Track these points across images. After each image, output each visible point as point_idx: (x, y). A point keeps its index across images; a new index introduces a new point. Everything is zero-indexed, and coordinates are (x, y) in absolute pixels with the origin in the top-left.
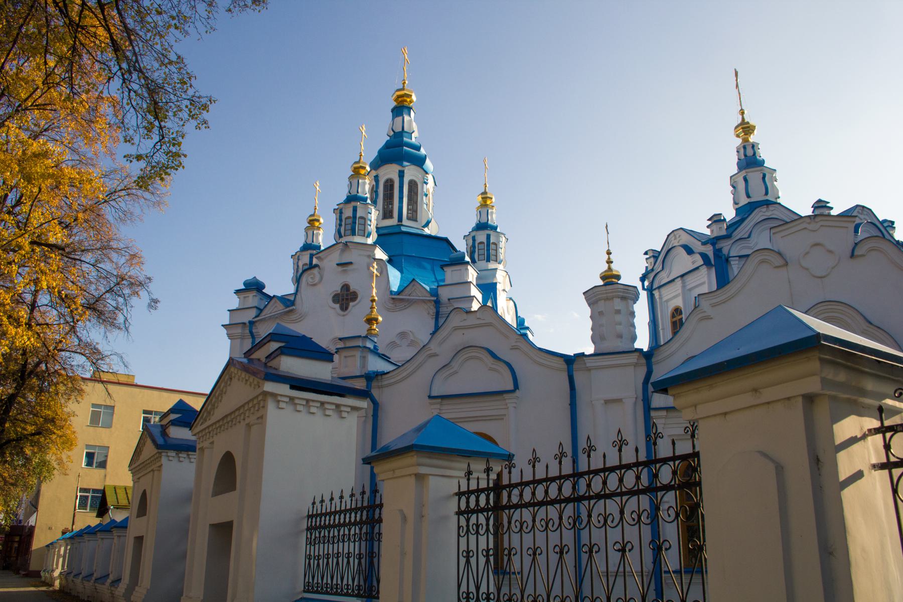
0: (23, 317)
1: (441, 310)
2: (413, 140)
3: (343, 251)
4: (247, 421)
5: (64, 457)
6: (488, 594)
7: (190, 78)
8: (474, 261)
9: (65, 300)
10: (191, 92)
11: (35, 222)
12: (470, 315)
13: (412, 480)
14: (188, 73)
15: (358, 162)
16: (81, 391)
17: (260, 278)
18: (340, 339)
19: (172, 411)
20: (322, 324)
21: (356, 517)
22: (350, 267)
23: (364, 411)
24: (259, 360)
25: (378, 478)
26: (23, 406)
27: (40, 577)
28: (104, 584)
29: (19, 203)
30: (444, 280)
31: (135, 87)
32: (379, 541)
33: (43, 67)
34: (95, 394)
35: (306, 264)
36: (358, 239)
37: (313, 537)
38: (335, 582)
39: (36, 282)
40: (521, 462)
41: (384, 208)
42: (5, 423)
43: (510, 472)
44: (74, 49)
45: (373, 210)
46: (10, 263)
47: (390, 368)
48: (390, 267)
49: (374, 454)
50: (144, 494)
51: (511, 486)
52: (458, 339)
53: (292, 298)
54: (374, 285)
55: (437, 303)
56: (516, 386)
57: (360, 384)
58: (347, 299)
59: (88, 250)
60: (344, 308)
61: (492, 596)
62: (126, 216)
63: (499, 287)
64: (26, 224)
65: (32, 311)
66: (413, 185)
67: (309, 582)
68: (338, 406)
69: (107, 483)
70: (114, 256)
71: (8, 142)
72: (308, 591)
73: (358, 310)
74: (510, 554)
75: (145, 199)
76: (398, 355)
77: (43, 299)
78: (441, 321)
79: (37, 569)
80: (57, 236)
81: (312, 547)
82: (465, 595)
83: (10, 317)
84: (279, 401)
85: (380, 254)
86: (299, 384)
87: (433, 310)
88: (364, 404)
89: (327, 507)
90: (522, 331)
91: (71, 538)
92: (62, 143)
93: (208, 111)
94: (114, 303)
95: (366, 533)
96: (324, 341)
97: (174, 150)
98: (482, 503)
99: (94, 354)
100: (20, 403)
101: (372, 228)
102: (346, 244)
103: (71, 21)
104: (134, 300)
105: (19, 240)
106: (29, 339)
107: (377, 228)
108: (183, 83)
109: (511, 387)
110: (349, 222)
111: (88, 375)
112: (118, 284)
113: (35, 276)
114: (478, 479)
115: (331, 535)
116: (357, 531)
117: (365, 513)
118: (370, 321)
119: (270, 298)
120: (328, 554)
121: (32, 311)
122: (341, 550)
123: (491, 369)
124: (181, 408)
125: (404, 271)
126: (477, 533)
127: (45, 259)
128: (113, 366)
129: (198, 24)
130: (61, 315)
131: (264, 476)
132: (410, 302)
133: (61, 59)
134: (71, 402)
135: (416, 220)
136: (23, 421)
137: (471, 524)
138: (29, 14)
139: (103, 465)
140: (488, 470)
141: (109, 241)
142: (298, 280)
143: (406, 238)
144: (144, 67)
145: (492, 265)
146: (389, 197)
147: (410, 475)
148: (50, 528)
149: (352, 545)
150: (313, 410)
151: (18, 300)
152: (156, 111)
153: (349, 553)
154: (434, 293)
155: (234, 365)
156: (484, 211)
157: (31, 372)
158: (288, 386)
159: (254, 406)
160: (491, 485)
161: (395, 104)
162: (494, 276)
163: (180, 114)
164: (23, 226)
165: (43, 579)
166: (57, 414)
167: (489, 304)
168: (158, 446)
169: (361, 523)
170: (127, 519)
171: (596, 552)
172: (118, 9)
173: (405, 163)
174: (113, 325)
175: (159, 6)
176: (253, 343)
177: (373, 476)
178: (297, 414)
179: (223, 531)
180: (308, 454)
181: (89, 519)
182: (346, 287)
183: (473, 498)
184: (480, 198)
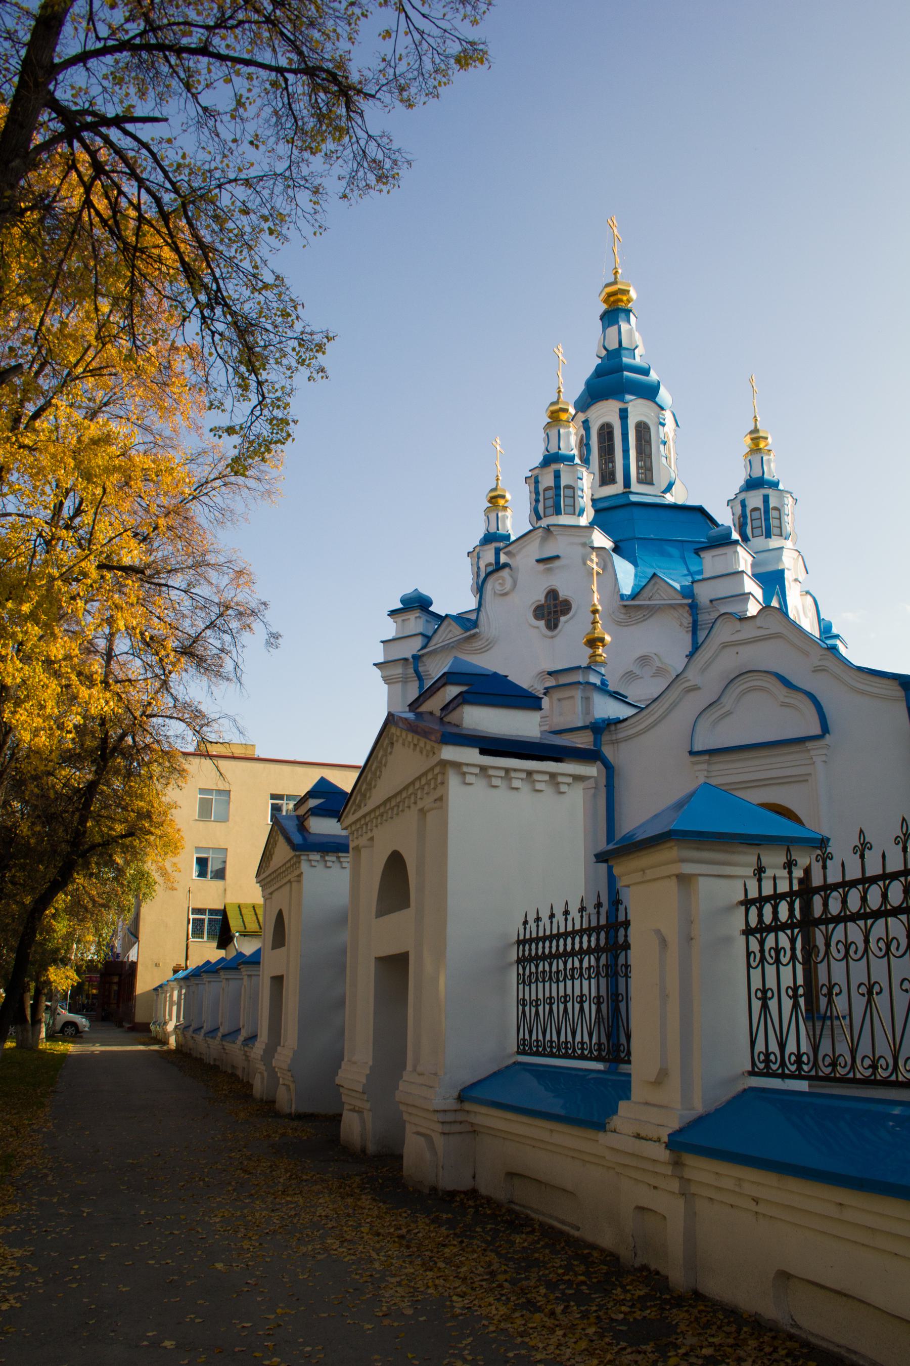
0: (96, 673)
1: (699, 618)
2: (638, 359)
3: (544, 540)
4: (420, 805)
5: (168, 866)
6: (799, 1056)
7: (295, 307)
8: (745, 539)
9: (151, 643)
10: (298, 327)
11: (102, 537)
12: (747, 625)
13: (673, 884)
14: (292, 300)
15: (557, 403)
16: (182, 772)
17: (425, 591)
18: (550, 674)
19: (311, 794)
20: (519, 652)
21: (589, 941)
22: (557, 563)
23: (592, 780)
24: (431, 713)
25: (620, 884)
26: (108, 797)
27: (150, 1031)
28: (234, 1042)
29: (78, 512)
30: (701, 572)
31: (220, 327)
32: (627, 976)
33: (93, 315)
34: (201, 773)
35: (490, 564)
36: (564, 520)
37: (527, 973)
38: (563, 1039)
39: (110, 621)
40: (842, 849)
41: (601, 469)
42: (86, 822)
43: (824, 867)
44: (132, 283)
45: (585, 473)
46: (73, 598)
47: (630, 711)
48: (616, 558)
49: (611, 847)
50: (280, 915)
51: (827, 888)
52: (729, 662)
53: (473, 617)
54: (595, 588)
55: (694, 608)
56: (825, 729)
57: (583, 741)
58: (555, 612)
59: (176, 570)
60: (552, 625)
61: (805, 1058)
62: (224, 515)
63: (787, 575)
64: (90, 542)
65: (108, 663)
66: (643, 430)
67: (524, 1039)
68: (553, 776)
69: (228, 901)
70: (212, 575)
71: (57, 428)
72: (524, 1053)
73: (573, 628)
74: (830, 994)
75: (250, 489)
76: (639, 692)
77: (122, 645)
78: (702, 635)
79: (145, 1021)
80: (132, 555)
81: (527, 988)
82: (762, 1057)
83: (79, 674)
84: (464, 774)
85: (600, 539)
86: (493, 746)
87: (687, 620)
88: (592, 770)
89: (546, 927)
90: (829, 642)
91: (186, 978)
92: (128, 419)
93: (324, 353)
94: (218, 644)
95: (607, 966)
96: (524, 677)
97: (280, 416)
98: (783, 915)
99: (195, 718)
100: (103, 792)
101: (585, 501)
102: (548, 529)
103: (125, 243)
104: (245, 637)
105: (83, 564)
106: (107, 702)
107: (593, 500)
108: (285, 314)
109: (816, 730)
110: (550, 498)
111: (191, 749)
112: (221, 615)
113: (108, 614)
114: (775, 878)
115: (554, 969)
116: (593, 962)
117: (603, 935)
118: (593, 642)
119: (441, 619)
120: (537, 1000)
121: (108, 663)
122: (569, 992)
123: (784, 705)
124: (323, 789)
125: (639, 561)
126: (778, 961)
127: (120, 588)
128: (224, 734)
129: (302, 223)
130: (148, 666)
131: (449, 886)
132: (652, 610)
133: (116, 302)
134: (170, 787)
135: (651, 483)
136: (109, 818)
137: (767, 948)
138: (70, 244)
139: (220, 874)
140: (789, 865)
141: (204, 555)
142: (480, 589)
143: (636, 511)
144: (230, 297)
145: (774, 543)
146: (607, 451)
147: (669, 877)
148: (157, 965)
149: (585, 983)
150: (516, 783)
151: (89, 649)
152: (251, 359)
153: (582, 996)
154: (688, 593)
155: (396, 725)
156: (756, 459)
157: (115, 749)
158: (477, 751)
159: (428, 783)
160: (796, 887)
161: (604, 307)
162: (779, 559)
163: (285, 362)
164: (86, 543)
165: (153, 1034)
166: (153, 807)
167: (775, 603)
168: (294, 847)
169: (596, 951)
170: (258, 952)
171: (877, 994)
172: (187, 218)
173: (628, 397)
174: (218, 674)
175: (244, 203)
176: (421, 686)
177: (612, 879)
178: (494, 790)
179: (395, 966)
180: (514, 850)
181: (207, 951)
182: (552, 594)
183: (768, 909)
184: (748, 440)
